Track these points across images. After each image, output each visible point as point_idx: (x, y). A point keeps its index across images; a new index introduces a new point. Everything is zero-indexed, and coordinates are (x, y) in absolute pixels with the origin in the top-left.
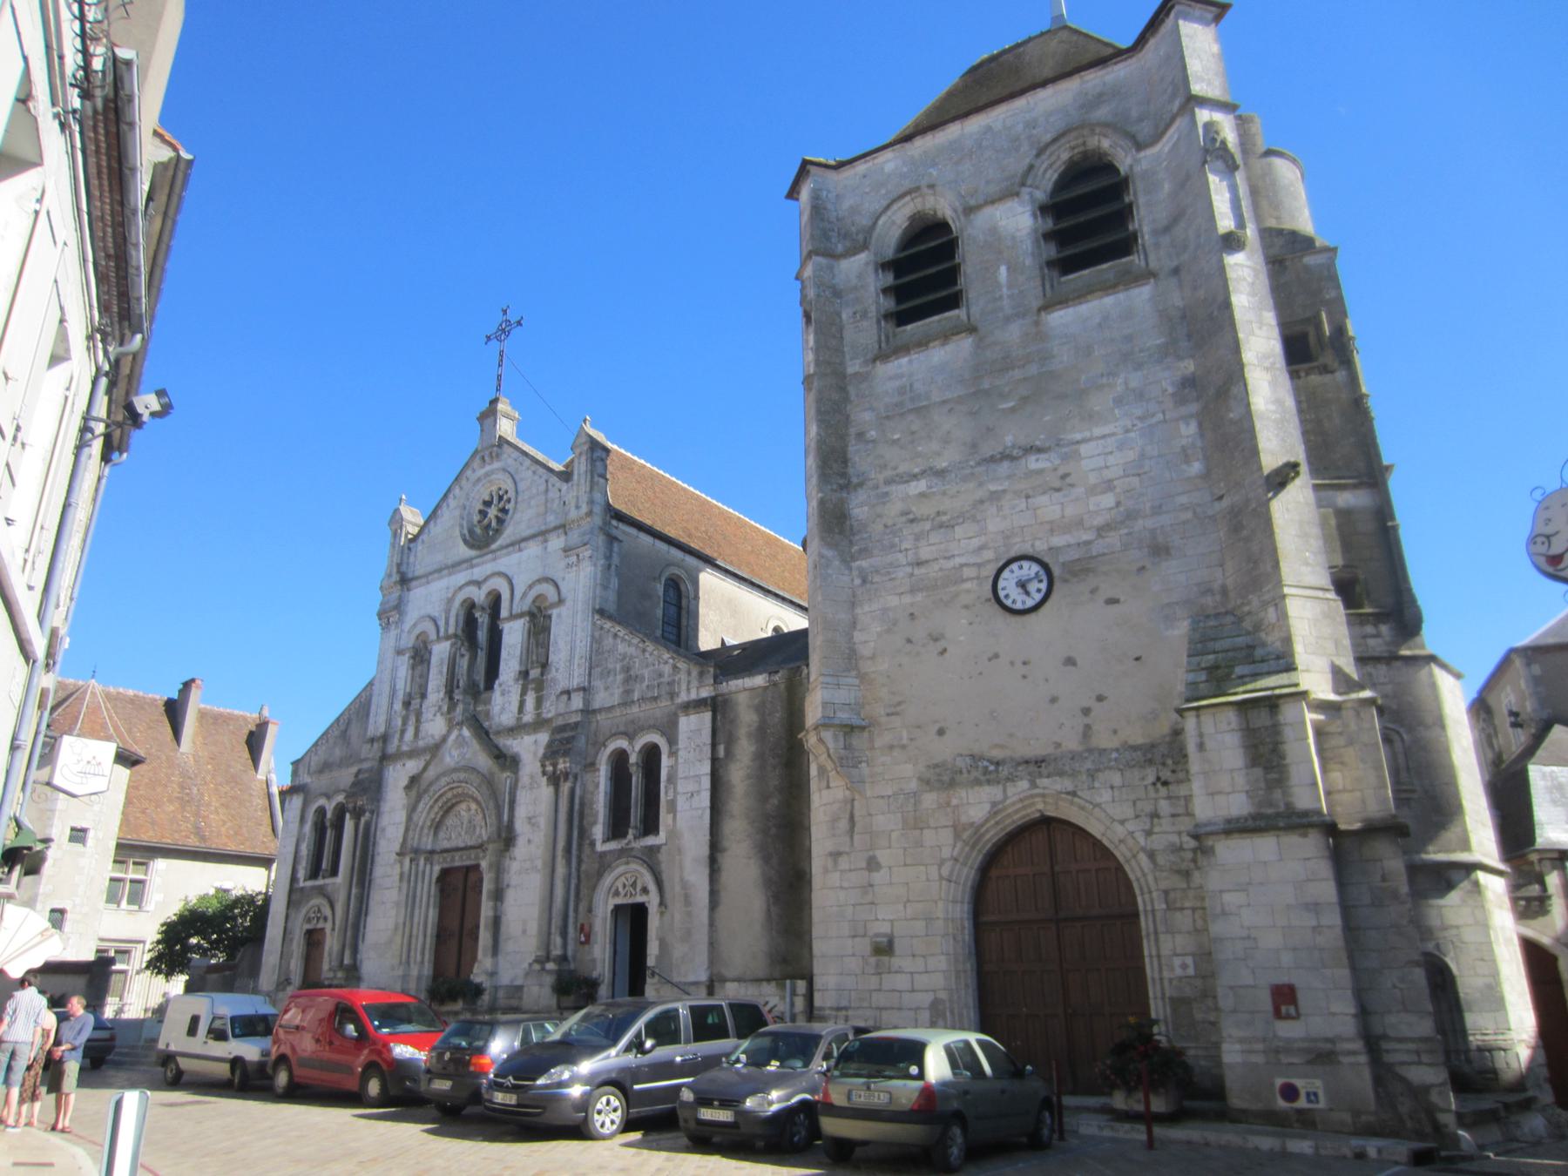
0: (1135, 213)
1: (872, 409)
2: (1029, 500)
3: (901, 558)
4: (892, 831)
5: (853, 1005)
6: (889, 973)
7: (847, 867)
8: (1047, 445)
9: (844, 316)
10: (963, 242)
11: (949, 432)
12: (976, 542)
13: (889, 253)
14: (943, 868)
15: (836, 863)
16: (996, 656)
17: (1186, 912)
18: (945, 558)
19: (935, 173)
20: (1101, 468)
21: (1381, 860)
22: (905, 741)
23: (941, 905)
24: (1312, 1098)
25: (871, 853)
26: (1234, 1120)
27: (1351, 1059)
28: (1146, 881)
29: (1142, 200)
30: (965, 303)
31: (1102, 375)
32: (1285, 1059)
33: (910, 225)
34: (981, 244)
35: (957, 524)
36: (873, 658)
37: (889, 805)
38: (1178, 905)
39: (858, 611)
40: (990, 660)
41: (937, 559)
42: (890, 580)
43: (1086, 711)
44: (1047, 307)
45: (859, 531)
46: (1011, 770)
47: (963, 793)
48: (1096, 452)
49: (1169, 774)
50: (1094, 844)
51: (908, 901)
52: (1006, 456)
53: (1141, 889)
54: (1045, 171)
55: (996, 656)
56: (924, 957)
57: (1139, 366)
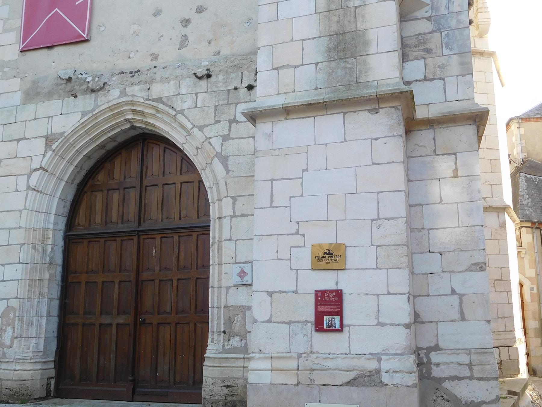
21: (455, 154)
43: (186, 22)
50: (182, 159)
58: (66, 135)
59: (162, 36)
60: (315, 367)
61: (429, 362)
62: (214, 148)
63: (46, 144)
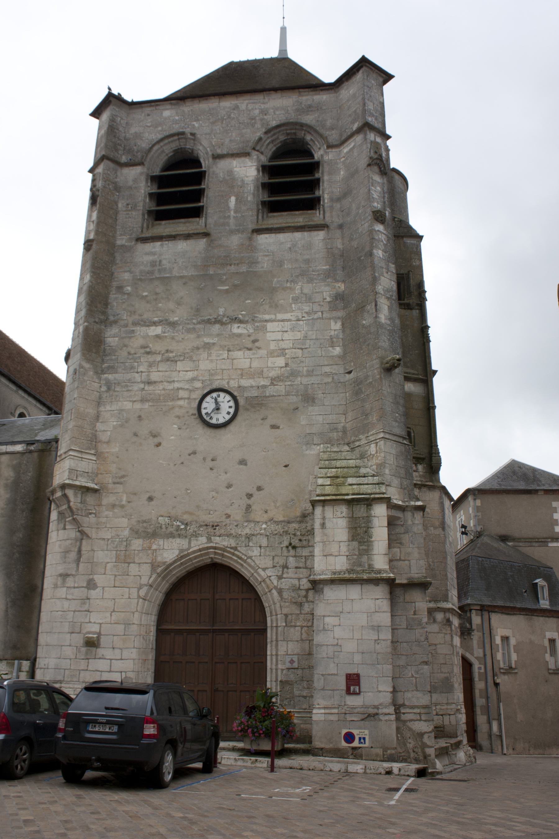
0: (321, 184)
1: (130, 272)
2: (230, 353)
3: (137, 377)
4: (108, 563)
5: (65, 680)
6: (95, 658)
7: (72, 585)
8: (246, 319)
9: (120, 205)
10: (209, 175)
11: (182, 298)
12: (190, 375)
13: (157, 172)
14: (141, 590)
15: (64, 581)
16: (194, 453)
17: (297, 628)
18: (168, 382)
19: (196, 125)
20: (279, 340)
21: (415, 602)
22: (124, 503)
23: (137, 615)
24: (362, 741)
25: (91, 577)
26: (314, 755)
27: (387, 717)
28: (275, 607)
29: (326, 178)
30: (204, 215)
31: (287, 281)
32: (349, 718)
33: (174, 155)
34: (221, 179)
35: (179, 360)
36: (108, 442)
37: (107, 545)
38: (293, 624)
39: (102, 409)
40: (189, 455)
41: (162, 382)
42: (127, 391)
43: (249, 496)
44: (258, 231)
45: (110, 354)
46: (196, 529)
47: (161, 542)
48: (277, 329)
49: (297, 541)
51: (114, 611)
52: (218, 321)
53: (271, 612)
54: (268, 144)
55: (194, 453)
56: (121, 649)
57: (310, 281)
58: (167, 564)
59: (233, 503)
60: (347, 712)
61: (400, 712)
62: (273, 583)
63: (152, 568)
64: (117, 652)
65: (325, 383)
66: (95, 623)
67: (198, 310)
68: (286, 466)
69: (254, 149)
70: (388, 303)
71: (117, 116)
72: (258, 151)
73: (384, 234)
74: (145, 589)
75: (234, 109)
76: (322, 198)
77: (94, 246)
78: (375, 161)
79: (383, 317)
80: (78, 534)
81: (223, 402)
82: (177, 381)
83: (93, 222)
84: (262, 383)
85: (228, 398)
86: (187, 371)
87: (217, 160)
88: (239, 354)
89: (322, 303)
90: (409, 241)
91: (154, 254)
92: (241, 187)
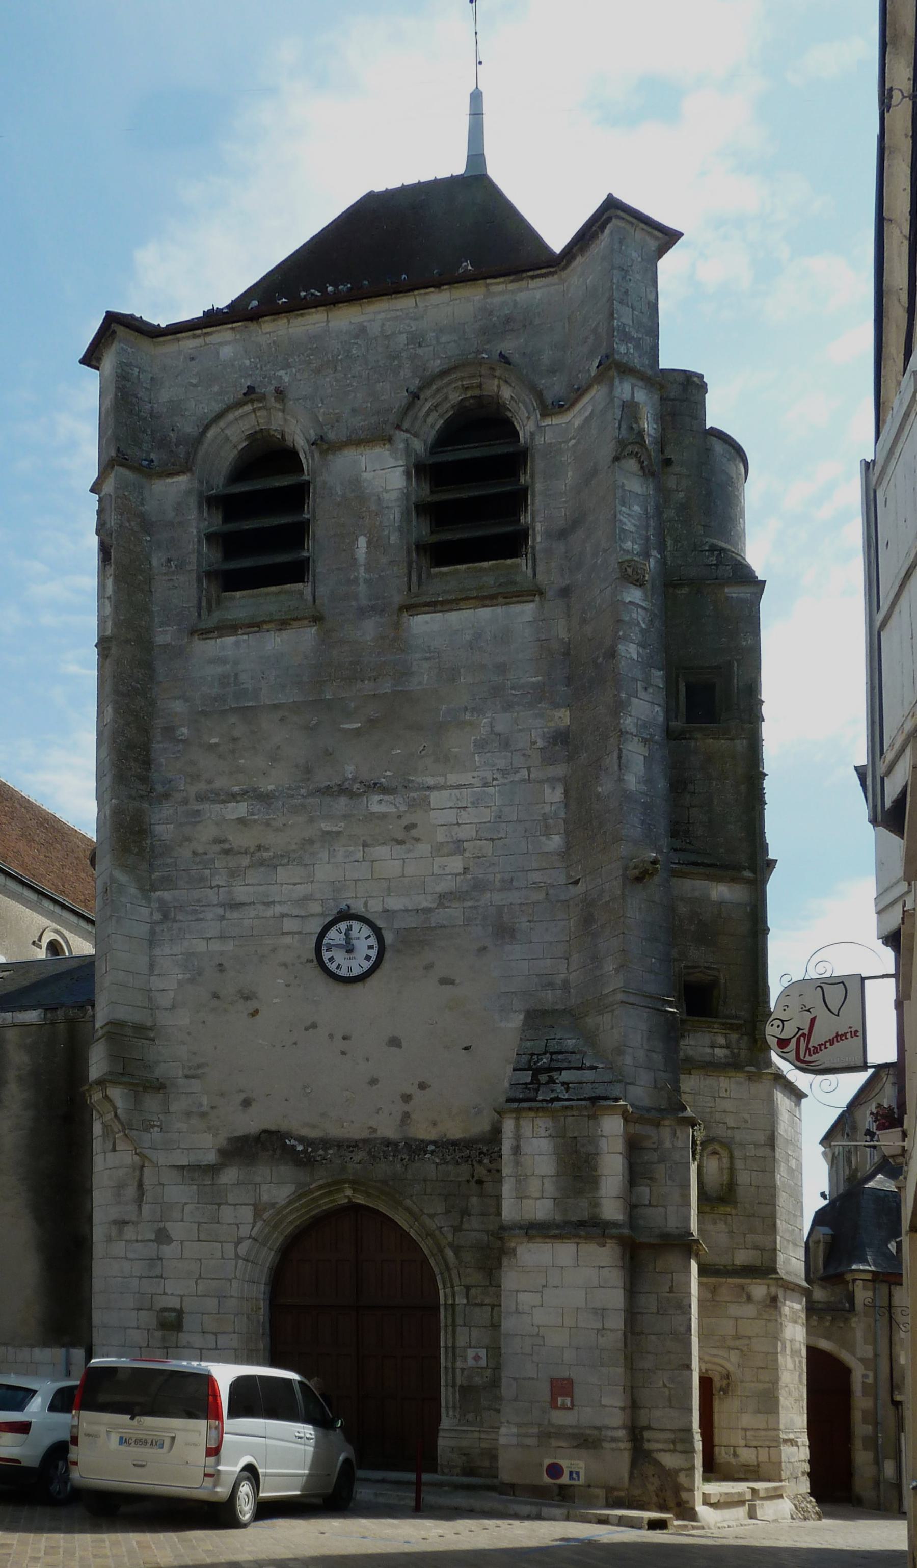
2: (366, 849)
3: (211, 895)
4: (186, 1204)
6: (177, 1347)
7: (134, 1238)
9: (155, 562)
10: (314, 489)
11: (279, 747)
13: (218, 484)
15: (120, 1232)
16: (314, 1026)
18: (264, 904)
25: (161, 1225)
29: (539, 487)
31: (466, 709)
35: (281, 865)
39: (157, 952)
41: (253, 903)
43: (407, 1098)
44: (411, 608)
51: (200, 1277)
52: (343, 790)
55: (314, 1026)
57: (508, 707)
58: (278, 1206)
61: (642, 1438)
64: (210, 1337)
65: (533, 903)
66: (172, 1294)
67: (308, 771)
68: (466, 1048)
69: (398, 427)
70: (642, 750)
71: (129, 365)
72: (407, 431)
73: (645, 609)
74: (246, 1244)
75: (357, 337)
76: (530, 532)
77: (114, 650)
78: (630, 448)
79: (632, 782)
80: (137, 1158)
81: (358, 938)
82: (279, 902)
83: (109, 598)
84: (425, 904)
85: (366, 931)
86: (295, 884)
87: (330, 457)
88: (382, 851)
89: (528, 752)
90: (733, 592)
91: (223, 661)
92: (377, 514)
